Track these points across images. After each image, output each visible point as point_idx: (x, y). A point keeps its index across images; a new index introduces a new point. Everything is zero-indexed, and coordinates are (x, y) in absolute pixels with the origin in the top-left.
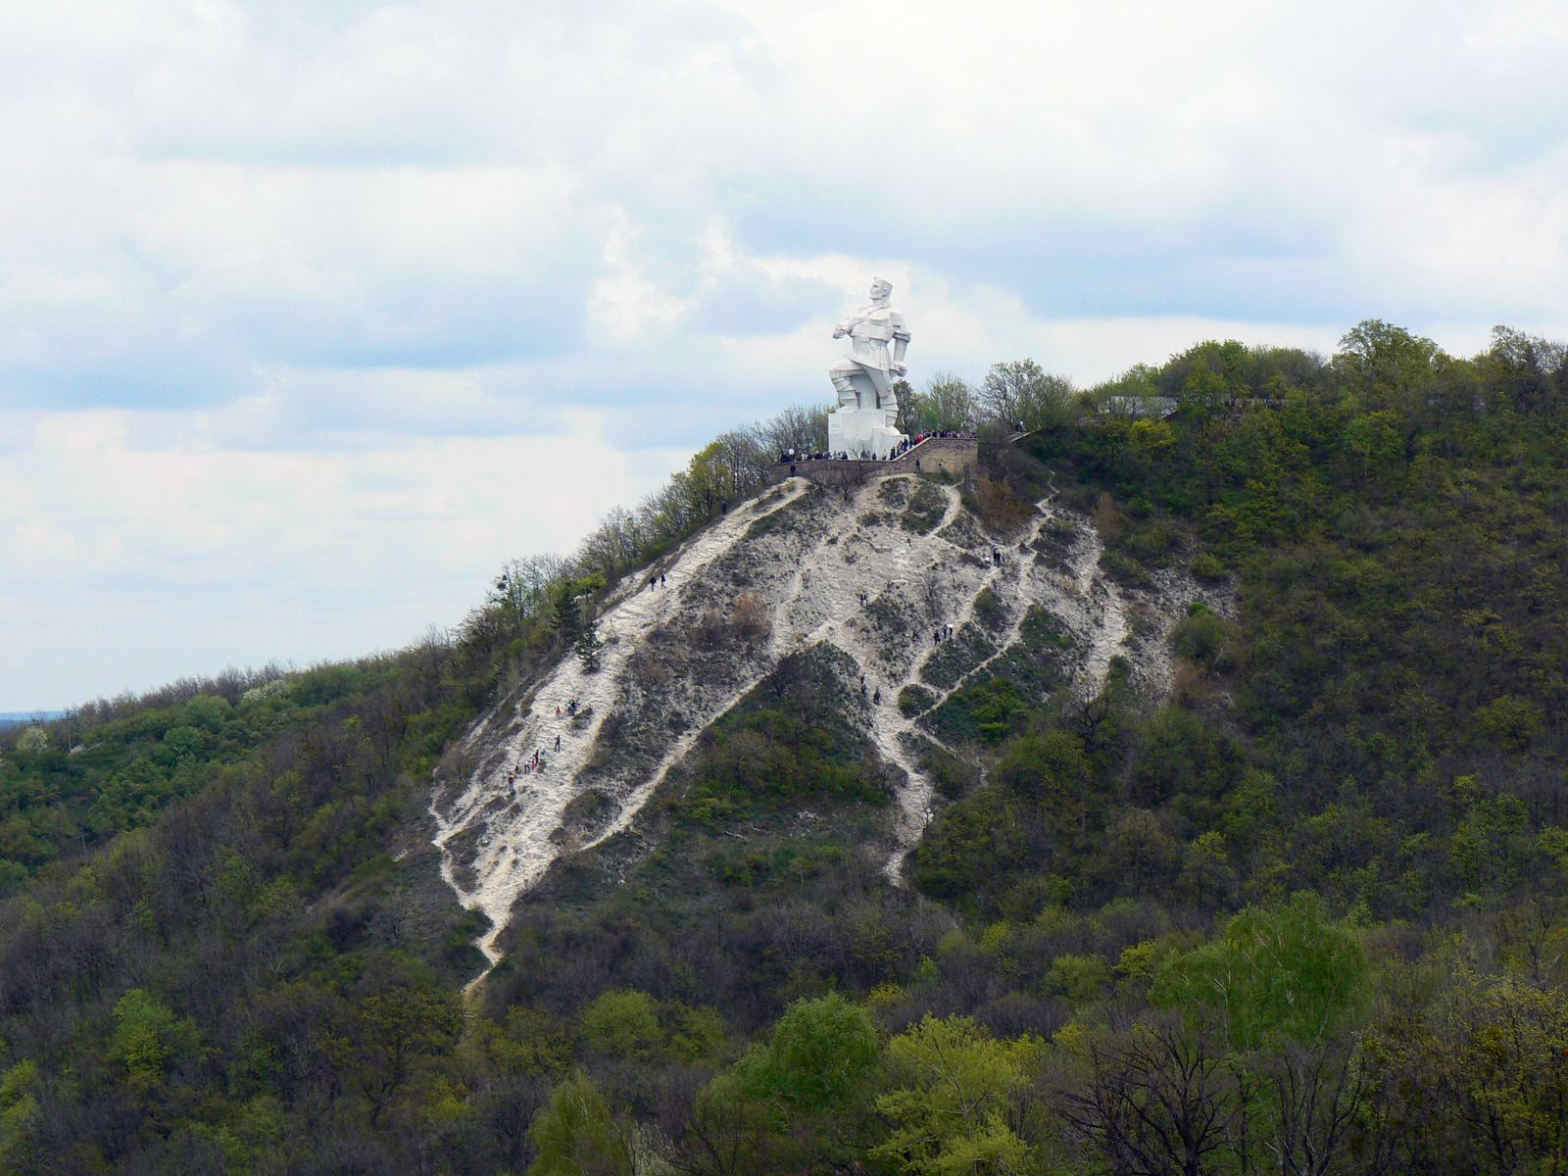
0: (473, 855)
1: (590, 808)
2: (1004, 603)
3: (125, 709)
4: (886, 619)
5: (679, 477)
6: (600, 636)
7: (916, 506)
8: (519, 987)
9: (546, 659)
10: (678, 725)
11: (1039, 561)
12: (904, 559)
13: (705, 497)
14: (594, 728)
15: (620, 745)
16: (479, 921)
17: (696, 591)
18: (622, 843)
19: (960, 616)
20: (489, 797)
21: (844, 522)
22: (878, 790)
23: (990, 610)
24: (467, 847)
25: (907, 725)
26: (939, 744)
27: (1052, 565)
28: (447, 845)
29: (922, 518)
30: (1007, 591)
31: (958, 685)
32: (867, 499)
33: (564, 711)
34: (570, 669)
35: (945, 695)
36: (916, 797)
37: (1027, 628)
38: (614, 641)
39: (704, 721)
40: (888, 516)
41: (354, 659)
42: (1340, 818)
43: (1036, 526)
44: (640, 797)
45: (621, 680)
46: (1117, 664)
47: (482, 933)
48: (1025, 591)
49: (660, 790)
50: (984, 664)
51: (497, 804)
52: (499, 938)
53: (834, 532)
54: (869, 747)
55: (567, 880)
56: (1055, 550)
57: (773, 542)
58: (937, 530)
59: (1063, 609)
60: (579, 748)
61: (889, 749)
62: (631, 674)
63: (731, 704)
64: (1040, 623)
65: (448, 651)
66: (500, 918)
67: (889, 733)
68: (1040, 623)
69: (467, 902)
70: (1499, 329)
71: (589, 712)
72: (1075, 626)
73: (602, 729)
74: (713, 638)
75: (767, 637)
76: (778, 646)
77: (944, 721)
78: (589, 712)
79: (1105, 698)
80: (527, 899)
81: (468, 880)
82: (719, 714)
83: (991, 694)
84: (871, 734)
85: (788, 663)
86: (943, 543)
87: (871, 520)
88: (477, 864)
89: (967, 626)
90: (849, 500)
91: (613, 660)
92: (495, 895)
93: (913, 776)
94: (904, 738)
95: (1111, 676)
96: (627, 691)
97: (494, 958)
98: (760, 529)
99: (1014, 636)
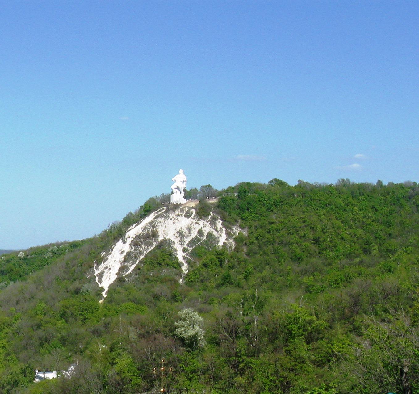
0: (102, 277)
1: (123, 269)
2: (203, 232)
3: (38, 248)
4: (180, 234)
5: (380, 182)
6: (126, 236)
7: (187, 213)
8: (110, 300)
9: (116, 240)
10: (141, 253)
11: (210, 224)
12: (184, 223)
13: (146, 211)
14: (125, 254)
15: (128, 257)
16: (102, 289)
17: (145, 228)
18: (130, 275)
19: (195, 234)
20: (105, 266)
21: (172, 215)
22: (180, 265)
23: (200, 232)
24: (101, 275)
25: (184, 254)
26: (190, 258)
27: (212, 225)
28: (97, 275)
29: (188, 215)
30: (203, 230)
31: (194, 247)
32: (178, 212)
33: (121, 249)
34: (120, 243)
35: (191, 249)
36: (185, 268)
37: (207, 236)
38: (129, 237)
39: (146, 252)
40: (181, 215)
41: (89, 238)
42: (266, 273)
43: (210, 217)
44: (133, 267)
45: (130, 245)
46: (224, 243)
47: (103, 292)
48: (207, 229)
49: (137, 266)
50: (199, 243)
51: (107, 267)
52: (106, 293)
53: (171, 218)
54: (177, 258)
55: (120, 280)
56: (213, 222)
57: (159, 219)
58: (191, 217)
59: (215, 233)
60: (121, 258)
61: (181, 259)
62: (132, 244)
63: (150, 250)
64: (210, 235)
65: (98, 238)
66: (106, 289)
67: (180, 255)
68: (210, 235)
69: (100, 286)
70: (299, 181)
71: (124, 251)
72: (216, 236)
73: (126, 254)
74: (150, 235)
75: (158, 236)
76: (160, 239)
77: (191, 254)
78: (124, 251)
79: (222, 249)
80: (111, 286)
81: (100, 282)
82: (148, 252)
83: (202, 248)
84: (177, 256)
85: (162, 242)
86: (192, 220)
87: (178, 215)
88: (102, 279)
89: (196, 236)
90: (174, 212)
91: (129, 241)
92: (106, 284)
93: (185, 264)
94: (183, 257)
95: (223, 246)
96: (131, 247)
97: (105, 296)
98: (156, 217)
99: (205, 238)
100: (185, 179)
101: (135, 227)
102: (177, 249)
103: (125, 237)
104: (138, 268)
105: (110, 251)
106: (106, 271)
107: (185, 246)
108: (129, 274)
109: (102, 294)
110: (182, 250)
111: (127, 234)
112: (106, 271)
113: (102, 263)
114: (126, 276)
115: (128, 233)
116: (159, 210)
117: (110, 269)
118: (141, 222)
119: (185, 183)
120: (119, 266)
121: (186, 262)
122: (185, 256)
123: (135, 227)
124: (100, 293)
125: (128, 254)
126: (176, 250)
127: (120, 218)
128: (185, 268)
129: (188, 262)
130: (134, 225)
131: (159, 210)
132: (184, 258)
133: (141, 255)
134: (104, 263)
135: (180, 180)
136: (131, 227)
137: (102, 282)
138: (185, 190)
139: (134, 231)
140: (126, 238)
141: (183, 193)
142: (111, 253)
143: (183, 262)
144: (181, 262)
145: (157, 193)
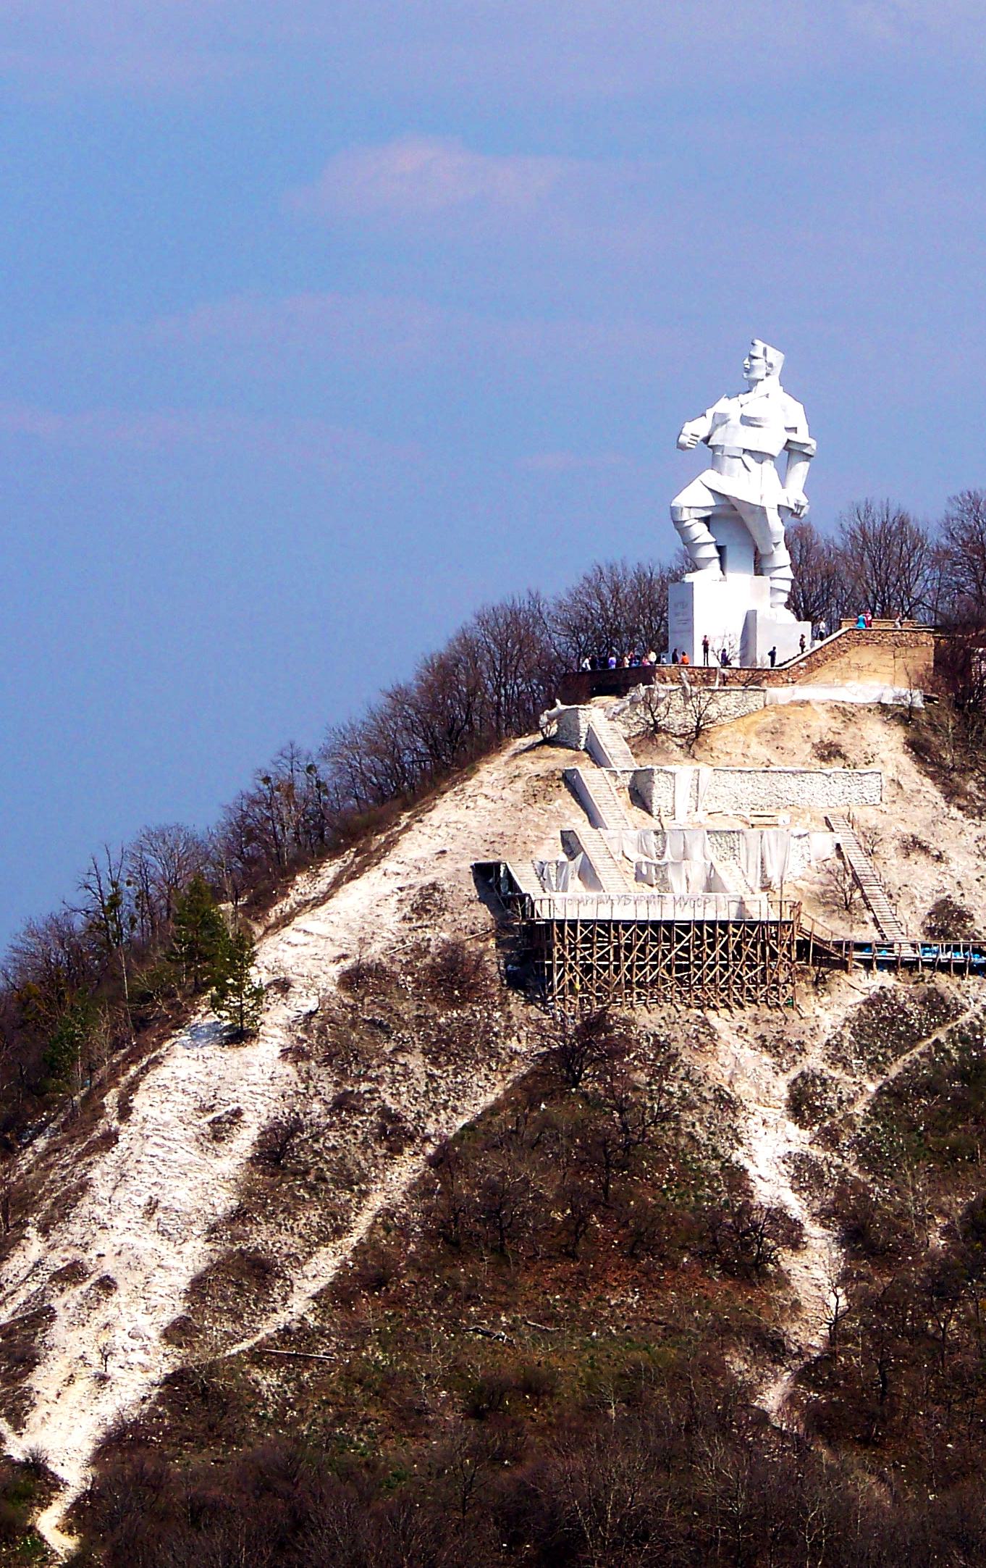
1: (241, 1275)
6: (258, 976)
14: (244, 1141)
16: (35, 1478)
20: (57, 1261)
36: (814, 1275)
44: (324, 1266)
45: (294, 1054)
47: (45, 1505)
50: (941, 1035)
51: (73, 1273)
54: (737, 1177)
60: (208, 1181)
61: (772, 1187)
66: (74, 1474)
67: (769, 1153)
80: (118, 1444)
84: (738, 1156)
93: (814, 1231)
100: (802, 436)
101: (336, 884)
102: (743, 1089)
103: (242, 977)
104: (364, 1280)
105: (99, 1112)
106: (66, 1301)
107: (814, 1060)
108: (520, 735)
109: (32, 1529)
110: (781, 1089)
111: (274, 954)
112: (66, 1301)
113: (31, 1232)
114: (258, 1356)
115: (271, 941)
116: (144, 1061)
117: (107, 1285)
118: (391, 843)
119: (801, 470)
120: (192, 1256)
121: (823, 1217)
122: (817, 1153)
123: (336, 884)
124: (10, 1509)
125: (276, 1151)
126: (727, 1103)
127: (204, 804)
128: (814, 1275)
129: (860, 1234)
130: (331, 870)
131: (144, 1061)
132: (805, 1173)
133: (395, 1150)
134: (44, 1230)
135: (758, 441)
136: (303, 886)
137: (34, 1418)
138: (800, 541)
139: (320, 937)
140: (258, 993)
141: (782, 556)
142: (110, 1139)
143: (796, 1207)
144: (778, 1215)
145: (550, 576)
